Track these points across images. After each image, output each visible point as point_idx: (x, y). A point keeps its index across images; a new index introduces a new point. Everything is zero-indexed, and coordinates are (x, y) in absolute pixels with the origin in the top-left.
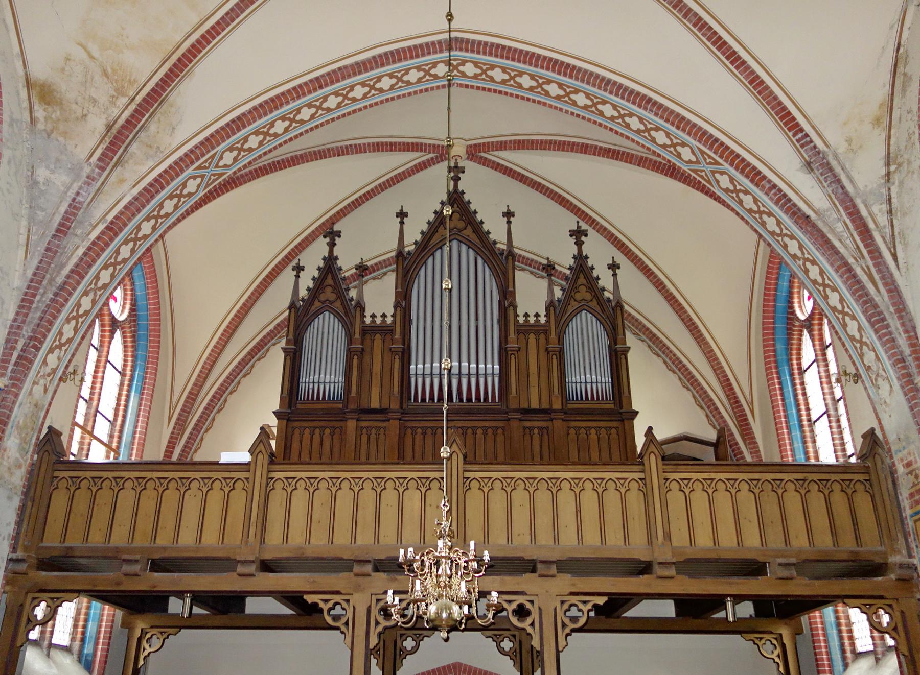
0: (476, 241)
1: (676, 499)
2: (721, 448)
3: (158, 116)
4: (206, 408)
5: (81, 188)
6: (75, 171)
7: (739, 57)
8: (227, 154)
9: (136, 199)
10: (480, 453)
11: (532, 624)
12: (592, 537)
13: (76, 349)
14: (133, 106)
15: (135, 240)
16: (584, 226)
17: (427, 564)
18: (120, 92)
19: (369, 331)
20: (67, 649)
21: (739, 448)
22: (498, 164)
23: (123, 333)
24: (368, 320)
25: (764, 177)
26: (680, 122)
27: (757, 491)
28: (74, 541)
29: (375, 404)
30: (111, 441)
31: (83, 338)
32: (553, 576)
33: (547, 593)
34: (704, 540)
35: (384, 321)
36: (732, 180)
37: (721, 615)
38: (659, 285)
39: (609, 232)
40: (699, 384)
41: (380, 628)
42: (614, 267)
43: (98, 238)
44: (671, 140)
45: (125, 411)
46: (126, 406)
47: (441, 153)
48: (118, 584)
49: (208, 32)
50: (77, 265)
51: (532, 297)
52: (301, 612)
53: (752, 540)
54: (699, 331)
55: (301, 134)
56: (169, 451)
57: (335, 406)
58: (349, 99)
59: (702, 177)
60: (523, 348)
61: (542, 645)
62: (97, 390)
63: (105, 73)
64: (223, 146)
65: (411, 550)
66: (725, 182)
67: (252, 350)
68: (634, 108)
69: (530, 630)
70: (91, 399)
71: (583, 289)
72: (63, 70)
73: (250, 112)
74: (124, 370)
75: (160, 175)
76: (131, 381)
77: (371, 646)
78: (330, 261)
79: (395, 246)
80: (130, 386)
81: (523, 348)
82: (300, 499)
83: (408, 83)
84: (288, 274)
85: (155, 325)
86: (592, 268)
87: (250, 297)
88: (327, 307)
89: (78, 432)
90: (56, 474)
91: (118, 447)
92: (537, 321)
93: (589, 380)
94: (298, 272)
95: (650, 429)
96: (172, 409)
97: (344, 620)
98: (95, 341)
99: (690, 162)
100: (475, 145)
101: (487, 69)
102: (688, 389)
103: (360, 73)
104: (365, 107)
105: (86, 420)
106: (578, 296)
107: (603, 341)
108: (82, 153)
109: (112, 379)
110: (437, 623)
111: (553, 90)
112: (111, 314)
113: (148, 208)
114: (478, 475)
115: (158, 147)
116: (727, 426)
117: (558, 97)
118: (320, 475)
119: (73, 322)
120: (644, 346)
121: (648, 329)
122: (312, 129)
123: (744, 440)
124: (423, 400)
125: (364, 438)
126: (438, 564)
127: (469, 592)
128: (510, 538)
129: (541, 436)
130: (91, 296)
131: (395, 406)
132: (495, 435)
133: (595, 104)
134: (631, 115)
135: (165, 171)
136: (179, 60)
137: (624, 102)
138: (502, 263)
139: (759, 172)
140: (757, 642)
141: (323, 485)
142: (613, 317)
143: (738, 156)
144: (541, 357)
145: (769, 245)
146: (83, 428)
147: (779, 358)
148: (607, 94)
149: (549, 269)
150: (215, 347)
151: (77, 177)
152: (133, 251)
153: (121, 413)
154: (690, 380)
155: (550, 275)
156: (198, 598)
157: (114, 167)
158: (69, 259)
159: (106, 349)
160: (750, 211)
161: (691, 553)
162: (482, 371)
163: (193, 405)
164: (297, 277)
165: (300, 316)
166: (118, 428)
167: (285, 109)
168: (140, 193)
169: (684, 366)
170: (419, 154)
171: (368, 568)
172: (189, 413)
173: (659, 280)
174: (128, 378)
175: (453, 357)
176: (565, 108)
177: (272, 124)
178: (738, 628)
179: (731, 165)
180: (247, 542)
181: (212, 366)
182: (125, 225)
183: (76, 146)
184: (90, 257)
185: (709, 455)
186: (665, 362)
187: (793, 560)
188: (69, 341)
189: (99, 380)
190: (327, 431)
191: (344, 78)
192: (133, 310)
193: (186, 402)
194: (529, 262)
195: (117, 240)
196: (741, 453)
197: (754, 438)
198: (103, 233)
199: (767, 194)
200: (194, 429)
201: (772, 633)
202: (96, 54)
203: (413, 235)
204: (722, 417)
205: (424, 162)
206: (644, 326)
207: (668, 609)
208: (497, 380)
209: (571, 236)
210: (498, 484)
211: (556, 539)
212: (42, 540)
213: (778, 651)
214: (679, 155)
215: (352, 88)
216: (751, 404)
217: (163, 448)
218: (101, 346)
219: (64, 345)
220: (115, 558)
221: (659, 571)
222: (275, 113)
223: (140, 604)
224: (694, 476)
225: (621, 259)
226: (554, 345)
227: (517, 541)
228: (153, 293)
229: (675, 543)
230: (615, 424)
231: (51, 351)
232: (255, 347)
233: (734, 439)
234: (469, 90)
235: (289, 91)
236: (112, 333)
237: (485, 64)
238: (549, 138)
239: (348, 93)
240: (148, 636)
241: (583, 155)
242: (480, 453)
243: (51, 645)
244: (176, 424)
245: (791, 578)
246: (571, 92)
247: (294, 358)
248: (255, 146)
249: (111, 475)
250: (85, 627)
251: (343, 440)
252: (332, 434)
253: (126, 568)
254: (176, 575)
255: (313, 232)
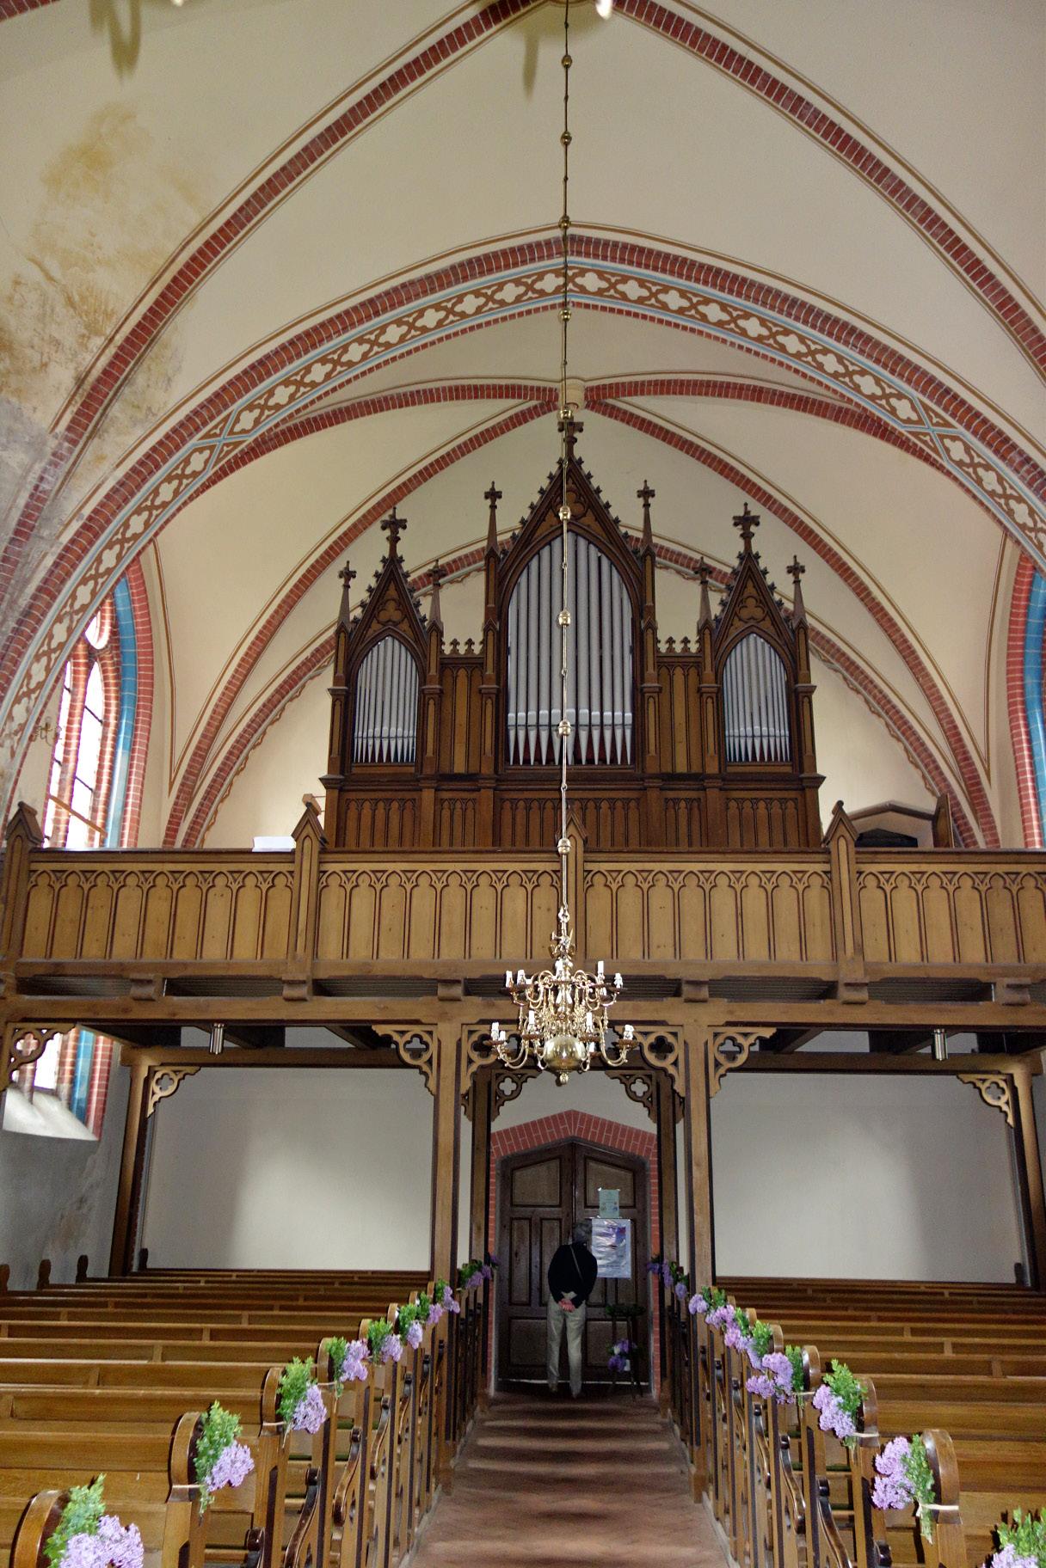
0: (603, 537)
1: (872, 899)
2: (941, 824)
3: (146, 362)
4: (220, 769)
5: (45, 470)
6: (36, 446)
7: (984, 269)
8: (245, 414)
9: (121, 484)
10: (605, 833)
11: (675, 1064)
12: (757, 950)
13: (49, 697)
14: (112, 350)
15: (122, 542)
16: (756, 509)
17: (541, 989)
18: (92, 329)
19: (450, 665)
20: (54, 1093)
21: (966, 824)
22: (632, 415)
23: (103, 665)
24: (447, 649)
25: (1014, 447)
26: (895, 363)
27: (983, 888)
28: (64, 955)
29: (459, 767)
30: (94, 817)
31: (57, 680)
32: (704, 1001)
33: (696, 1025)
34: (908, 953)
35: (470, 650)
36: (968, 449)
37: (927, 1050)
38: (861, 591)
39: (792, 514)
40: (914, 733)
41: (474, 1068)
42: (796, 570)
43: (72, 541)
44: (883, 389)
45: (111, 775)
46: (112, 768)
47: (547, 400)
48: (126, 1011)
49: (214, 237)
50: (46, 581)
51: (679, 613)
52: (360, 1044)
53: (974, 953)
54: (917, 658)
55: (349, 381)
56: (172, 831)
57: (405, 769)
58: (417, 329)
59: (925, 442)
60: (666, 690)
61: (688, 1089)
62: (73, 748)
63: (70, 302)
64: (240, 403)
65: (521, 973)
66: (957, 451)
67: (281, 687)
68: (831, 342)
69: (671, 1070)
70: (66, 760)
71: (751, 602)
72: (10, 299)
73: (276, 352)
74: (106, 717)
75: (154, 449)
76: (117, 732)
77: (463, 1090)
78: (393, 562)
79: (485, 533)
80: (116, 740)
81: (666, 690)
82: (363, 902)
83: (502, 303)
84: (330, 582)
85: (145, 654)
86: (765, 572)
87: (276, 612)
88: (389, 630)
89: (52, 804)
90: (34, 866)
91: (105, 825)
92: (686, 649)
93: (757, 733)
94: (347, 580)
95: (840, 804)
96: (173, 771)
97: (426, 1057)
98: (68, 683)
99: (909, 421)
100: (598, 387)
101: (617, 282)
102: (899, 740)
103: (433, 291)
104: (441, 340)
105: (61, 790)
106: (744, 613)
107: (779, 676)
108: (43, 419)
109: (91, 732)
110: (555, 1063)
111: (714, 313)
112: (87, 642)
113: (139, 496)
114: (604, 867)
115: (149, 409)
116: (952, 792)
117: (720, 324)
118: (390, 867)
119: (44, 660)
120: (836, 678)
121: (844, 654)
122: (364, 374)
123: (975, 812)
124: (527, 761)
125: (446, 813)
126: (556, 991)
127: (595, 1024)
128: (647, 951)
129: (690, 810)
130: (66, 622)
131: (487, 769)
132: (626, 807)
133: (771, 337)
134: (825, 351)
135: (161, 443)
136: (175, 280)
137: (816, 333)
138: (635, 561)
139: (1007, 440)
140: (979, 1084)
141: (394, 880)
142: (793, 640)
143: (978, 414)
144: (691, 699)
145: (1018, 542)
146: (58, 800)
147: (1029, 697)
148: (790, 321)
149: (703, 572)
150: (230, 682)
151: (39, 454)
152: (119, 557)
153: (105, 778)
154: (901, 728)
155: (704, 583)
156: (234, 1029)
157: (89, 438)
158: (34, 572)
159: (81, 690)
160: (992, 494)
161: (891, 971)
162: (607, 721)
163: (202, 764)
164: (347, 587)
165: (351, 645)
166: (102, 799)
167: (327, 346)
168: (127, 476)
169: (894, 707)
170: (516, 401)
171: (458, 991)
172: (197, 776)
173: (862, 583)
174: (112, 728)
175: (568, 701)
176: (730, 339)
177: (308, 370)
178: (953, 1067)
179: (968, 427)
180: (294, 957)
181: (227, 711)
182: (108, 522)
183: (35, 409)
184: (63, 568)
185: (925, 834)
186: (867, 701)
187: (1027, 981)
188: (40, 685)
189: (75, 734)
190: (395, 805)
191: (409, 300)
192: (114, 633)
193: (192, 760)
194: (676, 558)
195: (98, 542)
196: (970, 829)
197: (988, 809)
198: (78, 534)
199: (1017, 471)
200: (204, 798)
201: (999, 1073)
202: (56, 274)
203: (511, 517)
204: (945, 780)
205: (523, 413)
206: (839, 650)
207: (860, 1043)
208: (628, 733)
209: (736, 524)
210: (630, 880)
211: (709, 951)
212: (21, 955)
213: (1007, 1096)
214: (893, 411)
215: (421, 313)
216: (986, 762)
217: (164, 824)
218: (75, 685)
219: (33, 691)
220: (121, 977)
221: (844, 994)
222: (313, 353)
223: (142, 1036)
224: (898, 868)
225: (808, 557)
226: (709, 684)
227: (656, 955)
228: (141, 608)
229: (869, 958)
230: (793, 794)
231: (17, 700)
232: (285, 682)
233: (961, 810)
234: (590, 312)
235: (331, 321)
236: (89, 667)
237: (613, 275)
238: (705, 378)
239: (415, 320)
240: (158, 1075)
241: (755, 404)
242: (605, 833)
243: (33, 1089)
244: (180, 791)
245: (1023, 1004)
246: (739, 317)
247: (346, 704)
248: (283, 401)
249: (107, 867)
250: (74, 1064)
251: (417, 820)
252: (402, 810)
253: (137, 991)
254: (202, 999)
255: (364, 516)
